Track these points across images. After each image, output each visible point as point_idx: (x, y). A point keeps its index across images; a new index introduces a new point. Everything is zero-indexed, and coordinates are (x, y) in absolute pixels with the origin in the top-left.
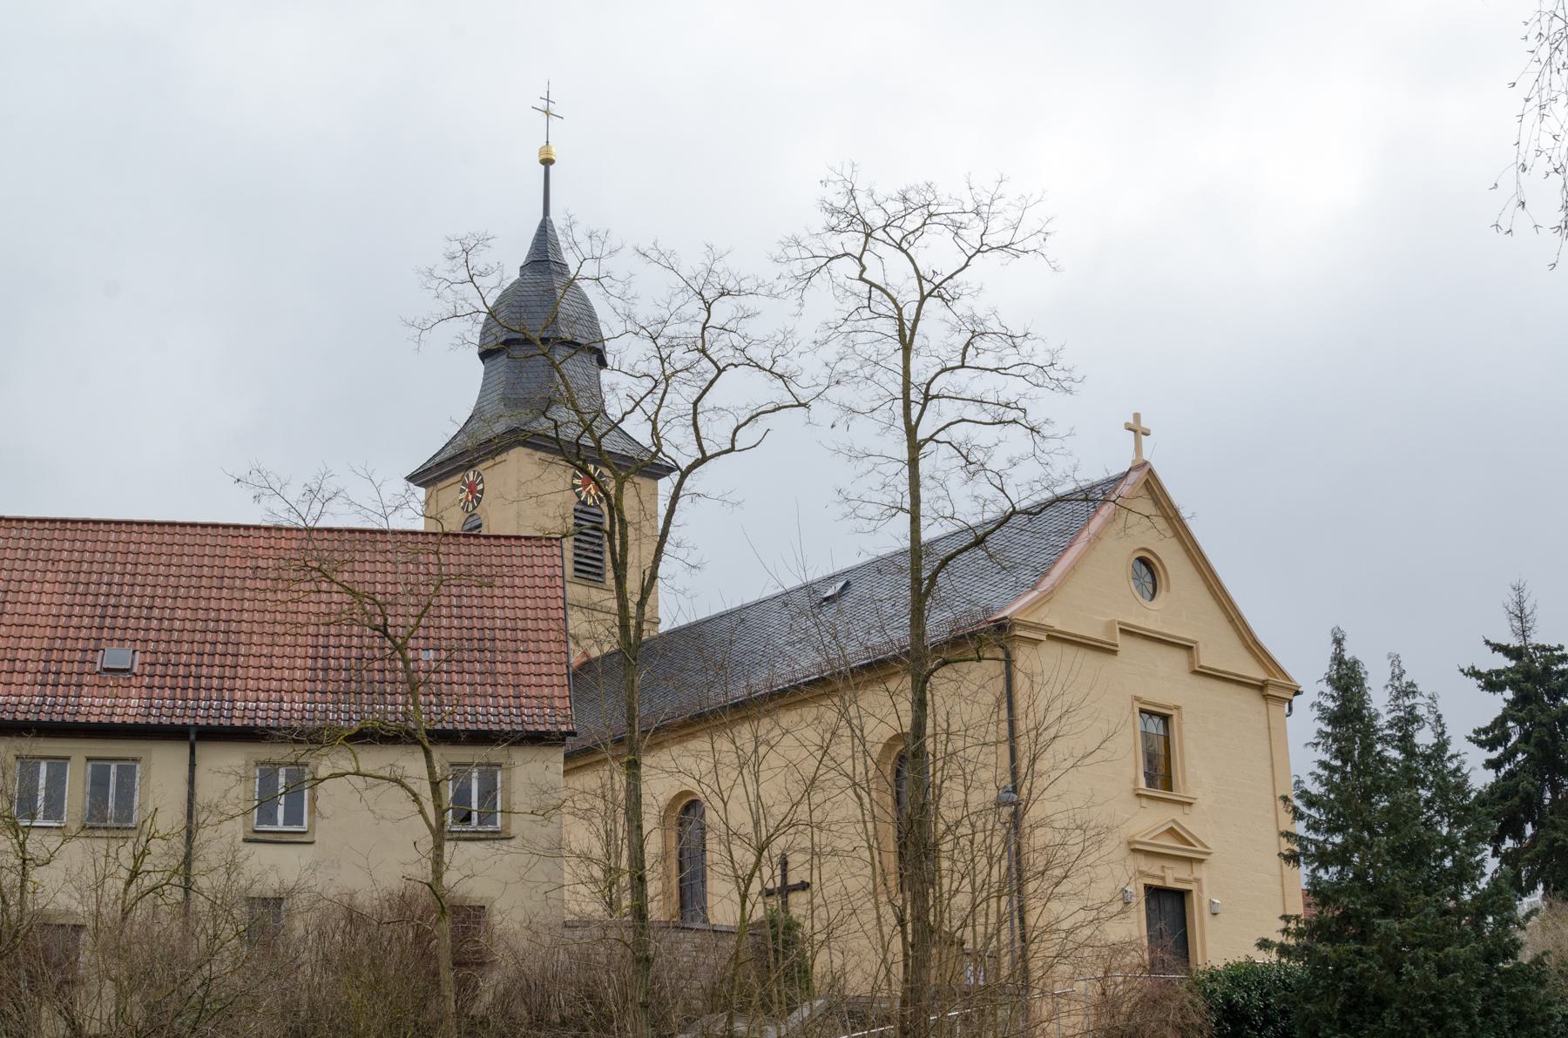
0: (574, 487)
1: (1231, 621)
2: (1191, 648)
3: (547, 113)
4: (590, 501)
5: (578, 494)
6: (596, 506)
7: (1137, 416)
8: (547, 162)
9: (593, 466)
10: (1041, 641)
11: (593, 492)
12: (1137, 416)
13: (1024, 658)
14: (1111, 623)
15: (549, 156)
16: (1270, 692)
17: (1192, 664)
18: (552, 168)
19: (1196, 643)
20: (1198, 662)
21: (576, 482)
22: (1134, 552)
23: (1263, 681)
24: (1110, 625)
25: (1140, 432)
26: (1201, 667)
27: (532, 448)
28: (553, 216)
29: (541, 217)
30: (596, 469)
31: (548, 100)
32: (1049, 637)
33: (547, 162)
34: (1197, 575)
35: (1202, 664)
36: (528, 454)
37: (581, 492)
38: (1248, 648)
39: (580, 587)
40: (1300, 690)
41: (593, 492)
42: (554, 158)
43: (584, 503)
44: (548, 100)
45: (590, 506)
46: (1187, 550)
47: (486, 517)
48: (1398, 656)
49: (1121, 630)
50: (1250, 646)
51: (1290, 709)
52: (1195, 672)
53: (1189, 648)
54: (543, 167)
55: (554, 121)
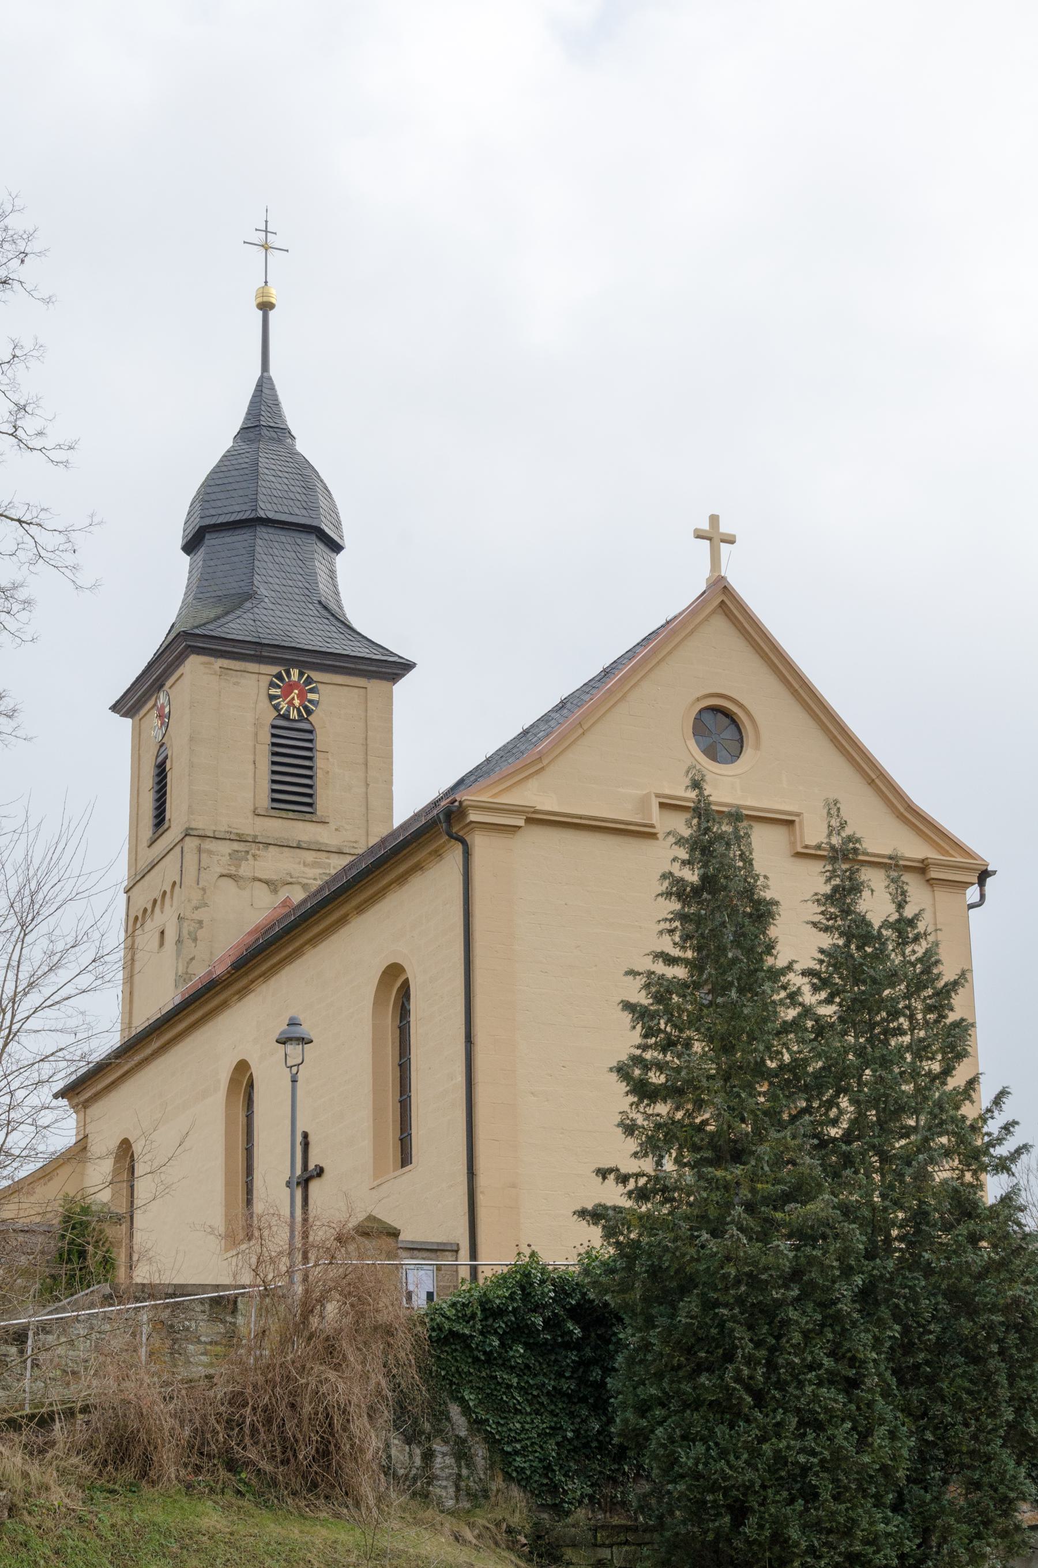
0: (272, 698)
1: (871, 782)
2: (792, 822)
3: (266, 247)
4: (293, 715)
5: (276, 708)
6: (301, 719)
7: (714, 520)
8: (266, 307)
9: (297, 671)
10: (519, 827)
11: (297, 702)
12: (714, 520)
13: (481, 844)
14: (648, 795)
15: (265, 299)
16: (933, 875)
17: (793, 844)
18: (272, 314)
19: (798, 815)
20: (801, 842)
21: (273, 691)
22: (693, 704)
23: (923, 861)
24: (644, 801)
25: (716, 540)
26: (806, 847)
27: (211, 655)
28: (274, 372)
29: (258, 373)
30: (301, 674)
31: (266, 231)
32: (529, 821)
33: (266, 307)
34: (811, 723)
35: (807, 843)
36: (203, 663)
37: (279, 704)
38: (900, 816)
39: (280, 820)
40: (990, 868)
41: (297, 702)
42: (273, 301)
43: (286, 717)
44: (266, 231)
45: (294, 720)
46: (795, 693)
47: (171, 745)
48: (836, 802)
49: (662, 805)
50: (902, 814)
51: (982, 896)
52: (798, 855)
53: (790, 823)
54: (261, 313)
55: (274, 256)
